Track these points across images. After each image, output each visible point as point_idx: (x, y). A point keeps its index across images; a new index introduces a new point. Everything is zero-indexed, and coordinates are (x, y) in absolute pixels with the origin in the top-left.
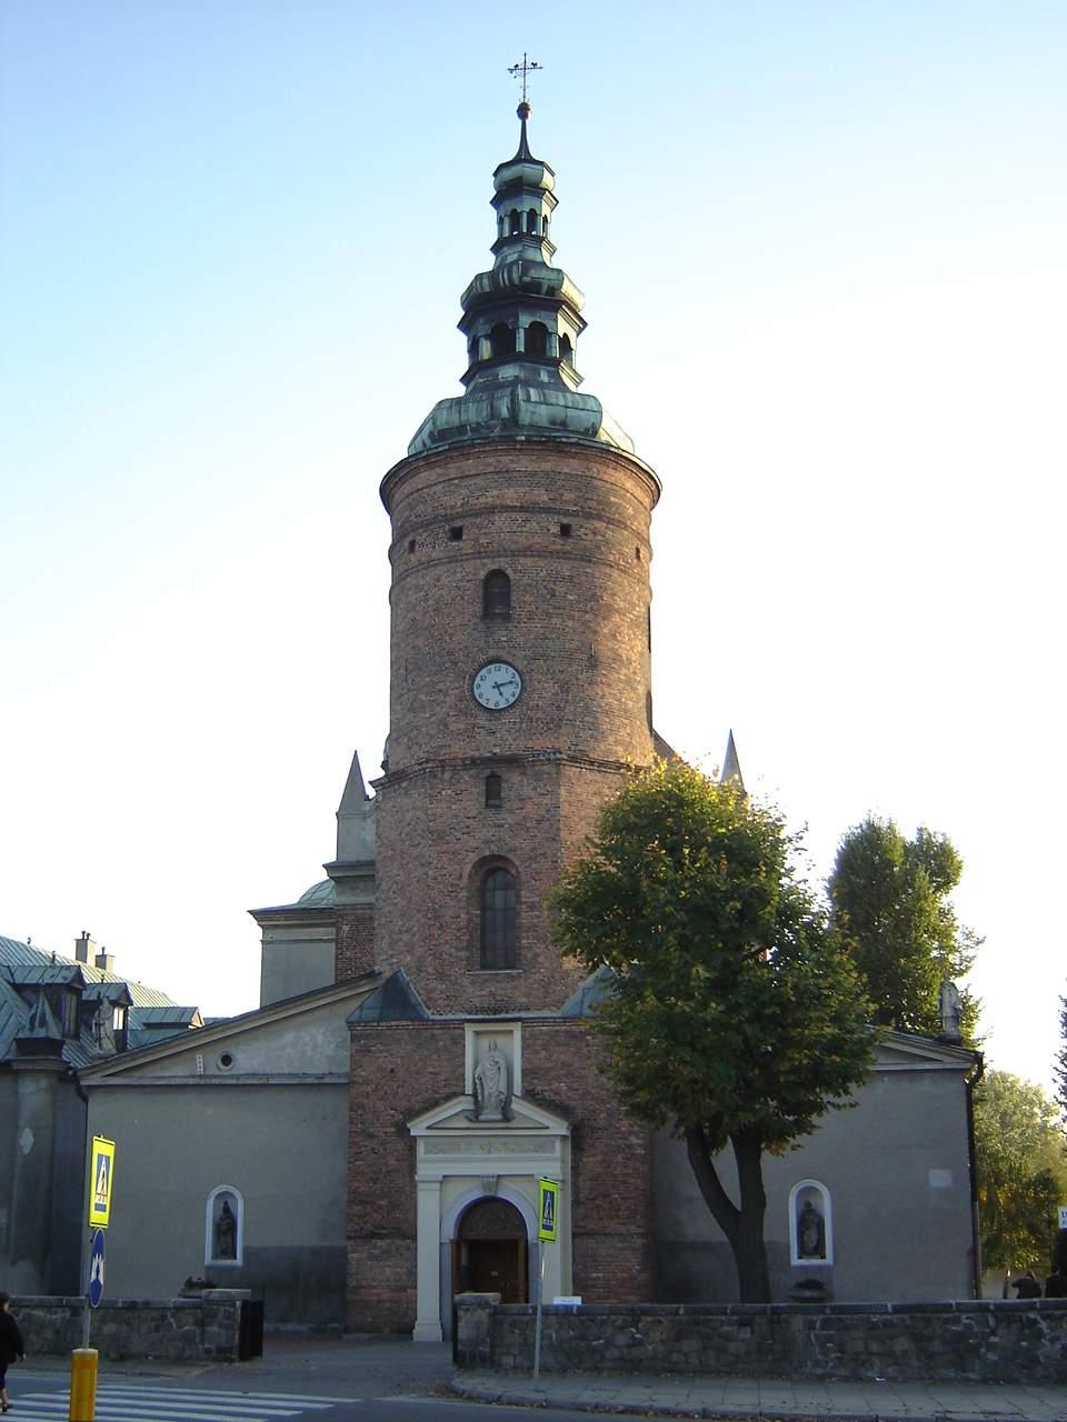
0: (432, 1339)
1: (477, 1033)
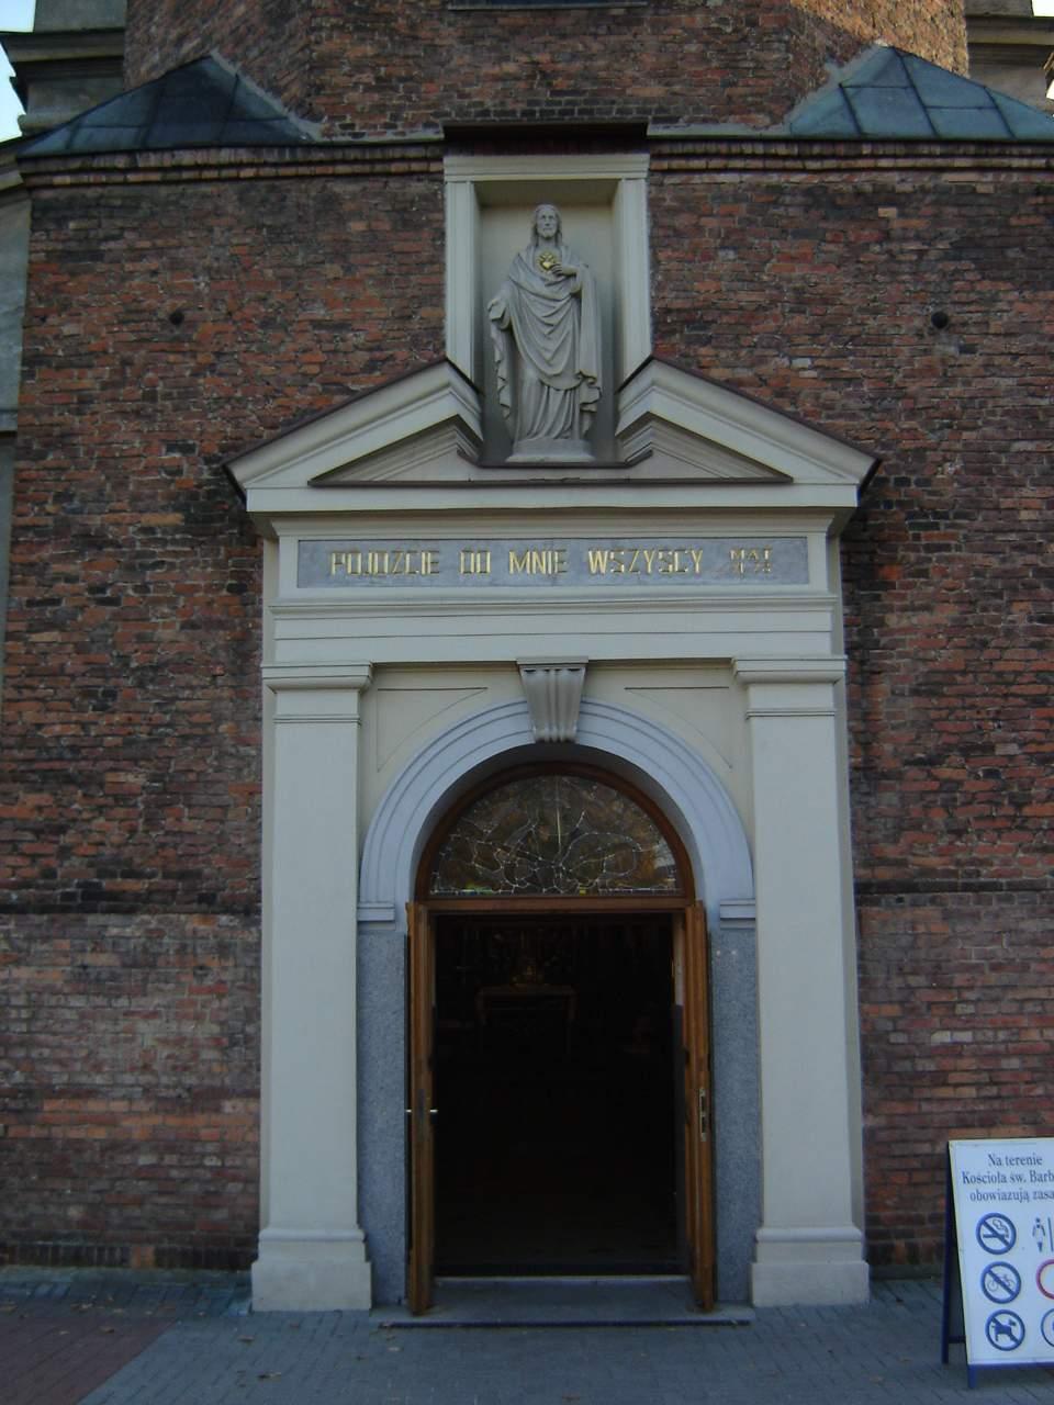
0: (331, 1301)
1: (489, 201)
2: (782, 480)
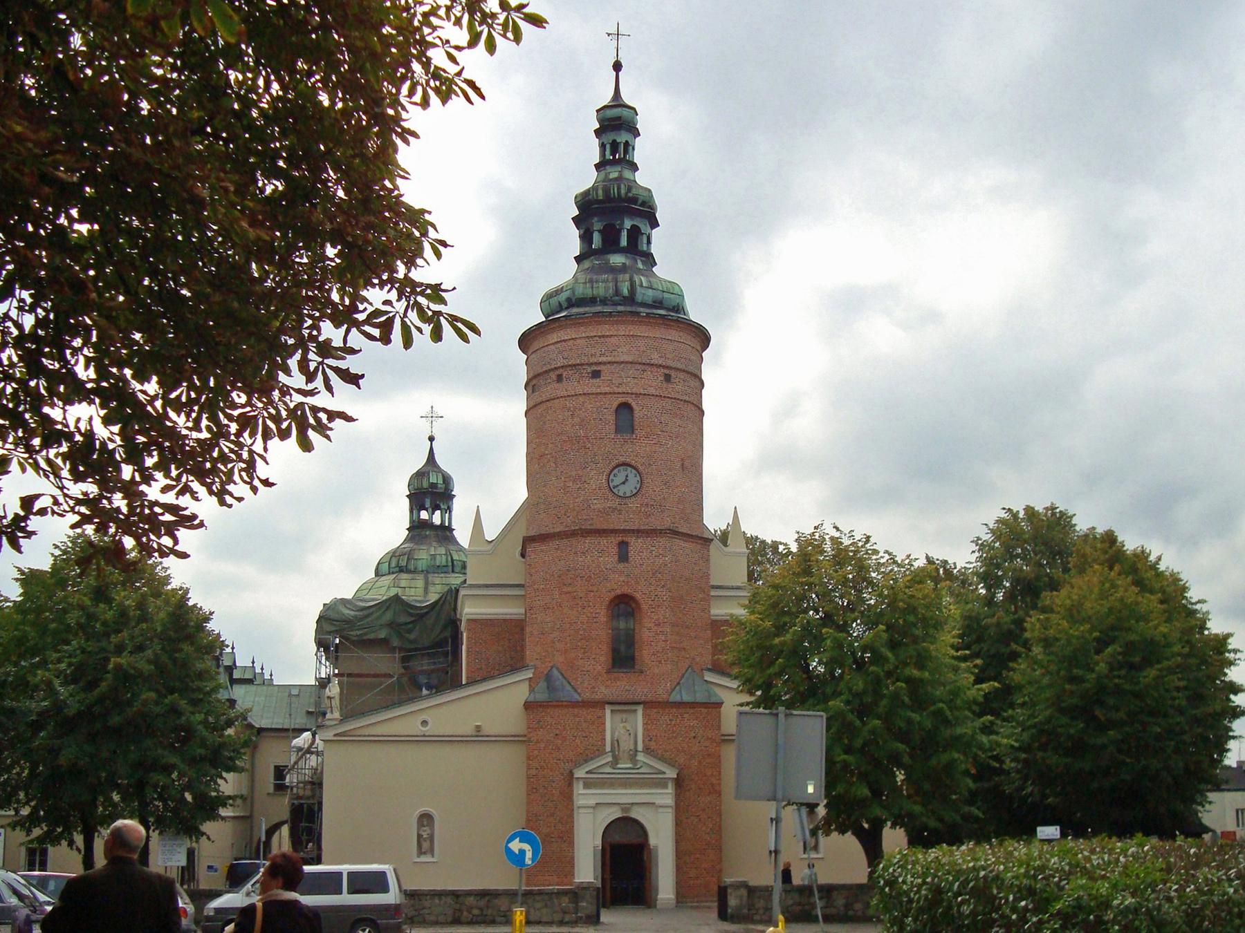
1: (612, 711)
2: (664, 773)
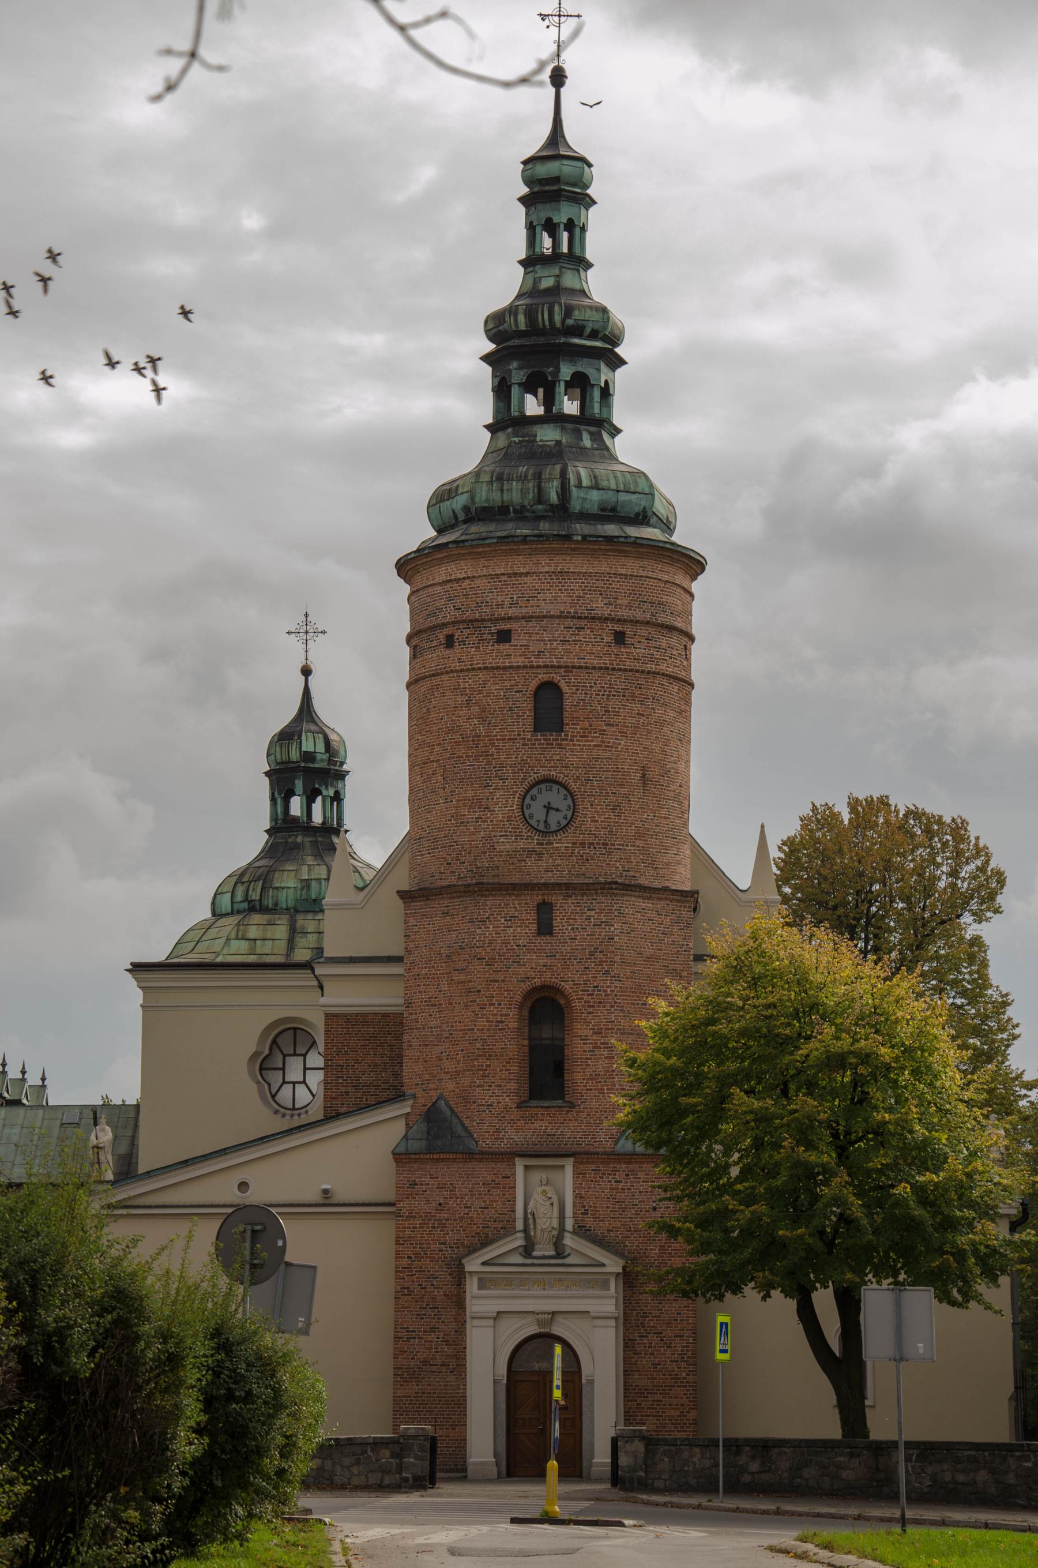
1: (526, 1167)
2: (604, 1265)
